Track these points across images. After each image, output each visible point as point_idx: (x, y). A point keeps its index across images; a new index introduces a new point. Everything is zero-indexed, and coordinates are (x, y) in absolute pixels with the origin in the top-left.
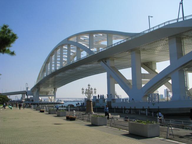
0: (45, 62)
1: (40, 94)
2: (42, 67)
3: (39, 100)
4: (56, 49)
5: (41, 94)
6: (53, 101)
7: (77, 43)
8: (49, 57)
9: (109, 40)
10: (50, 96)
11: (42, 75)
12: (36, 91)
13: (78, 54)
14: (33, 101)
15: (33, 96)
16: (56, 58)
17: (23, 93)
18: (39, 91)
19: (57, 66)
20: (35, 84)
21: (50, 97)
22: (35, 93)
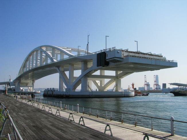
0: (25, 60)
1: (21, 85)
2: (23, 63)
3: (20, 89)
4: (33, 52)
5: (22, 85)
6: (31, 91)
7: (45, 51)
8: (28, 57)
9: (62, 56)
10: (29, 86)
11: (23, 69)
12: (18, 82)
13: (46, 60)
14: (14, 90)
15: (15, 86)
16: (33, 58)
17: (9, 84)
18: (20, 82)
19: (34, 63)
20: (17, 77)
21: (30, 88)
22: (17, 84)
